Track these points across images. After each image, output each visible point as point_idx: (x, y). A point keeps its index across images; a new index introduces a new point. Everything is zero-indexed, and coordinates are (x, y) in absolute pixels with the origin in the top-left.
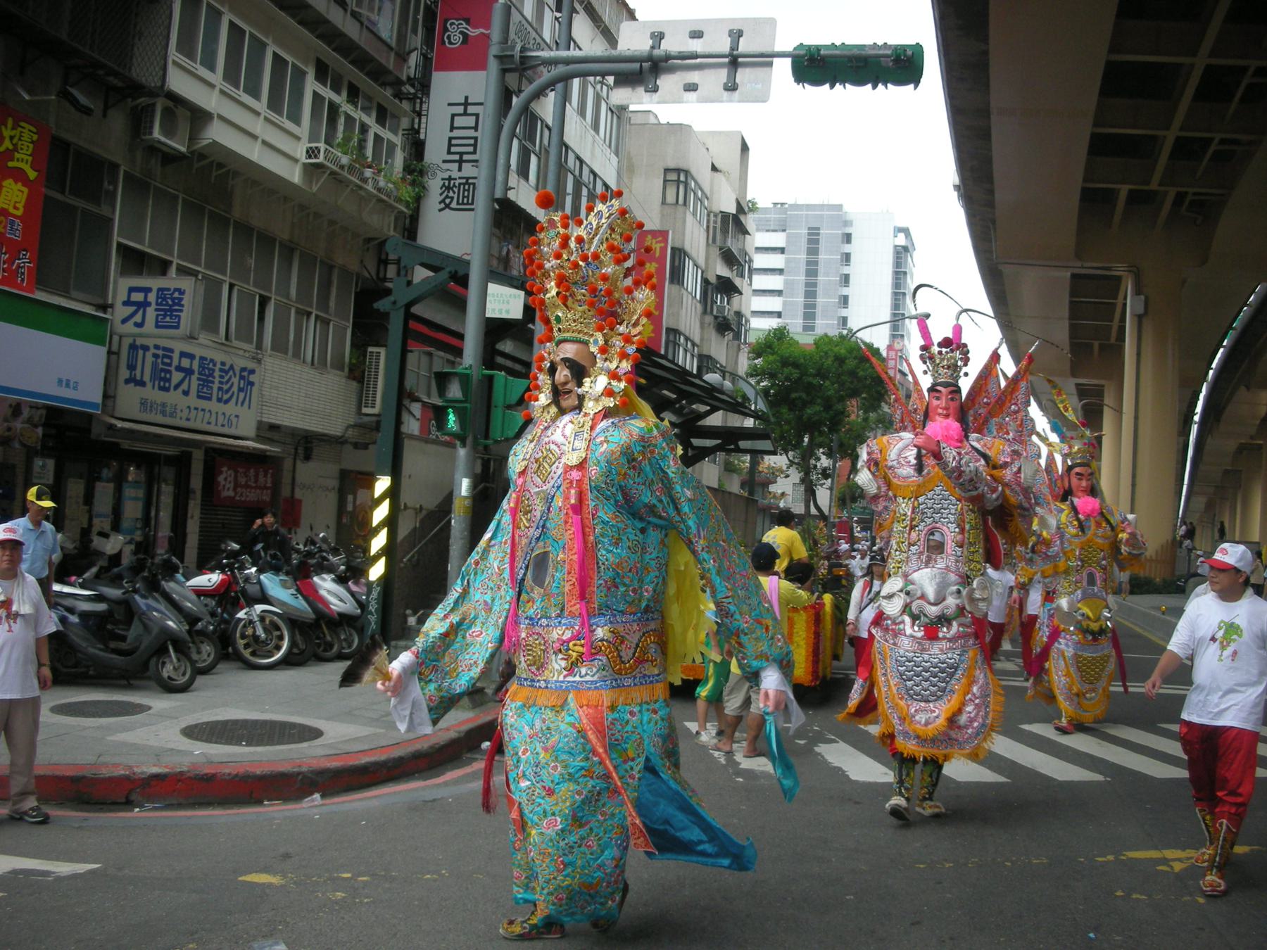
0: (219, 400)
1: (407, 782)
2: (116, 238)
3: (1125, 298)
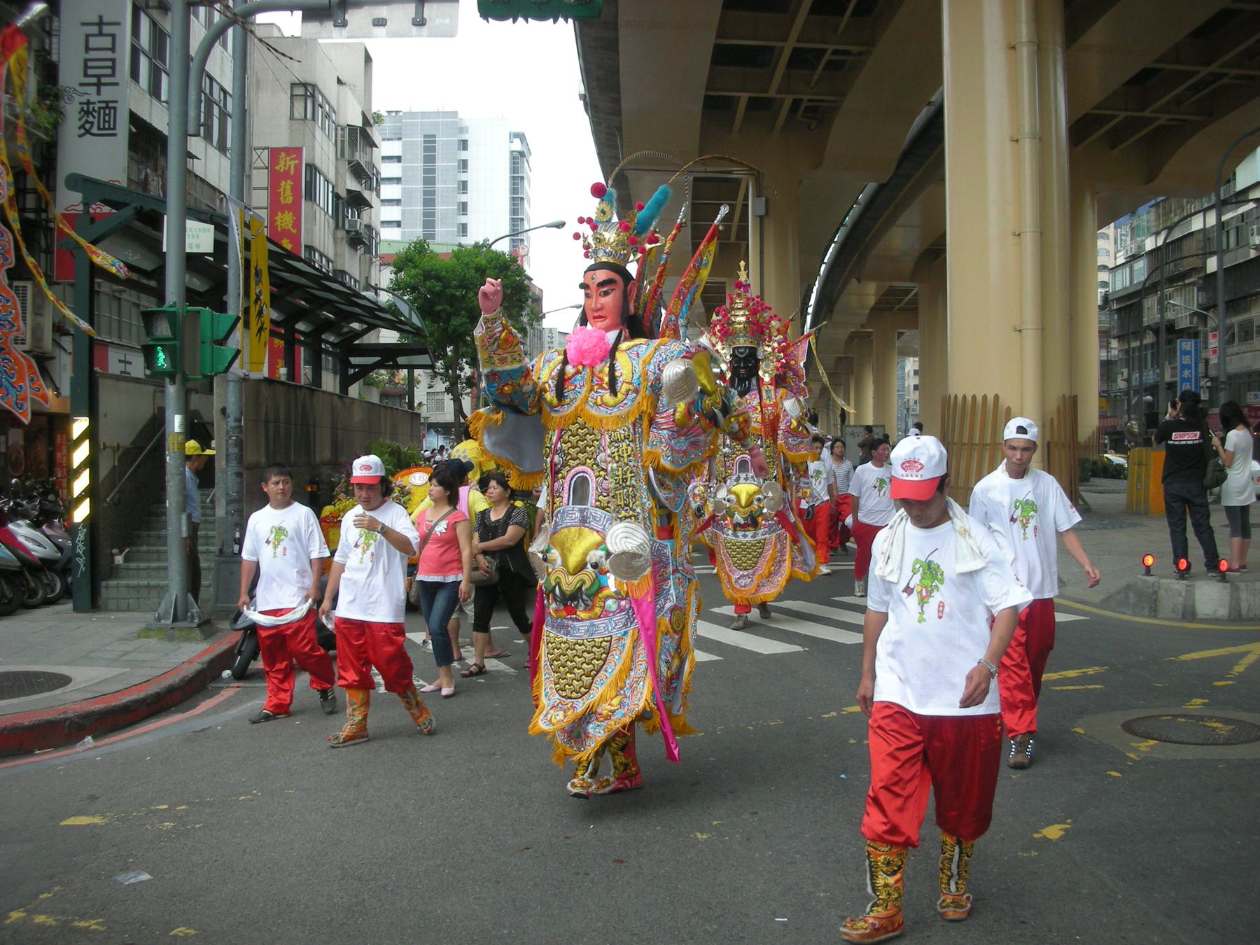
1: (167, 715)
3: (746, 198)
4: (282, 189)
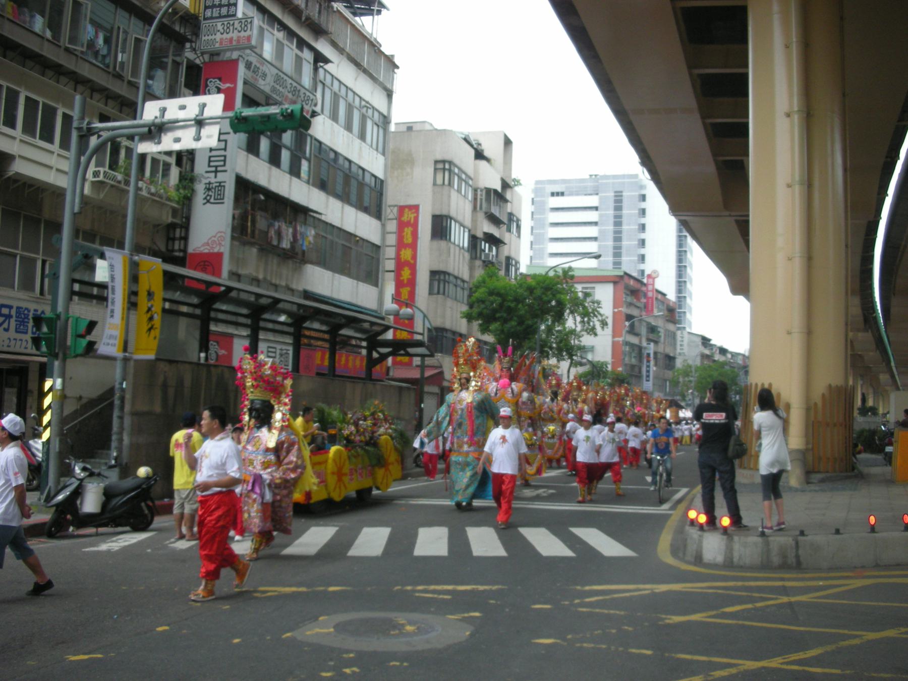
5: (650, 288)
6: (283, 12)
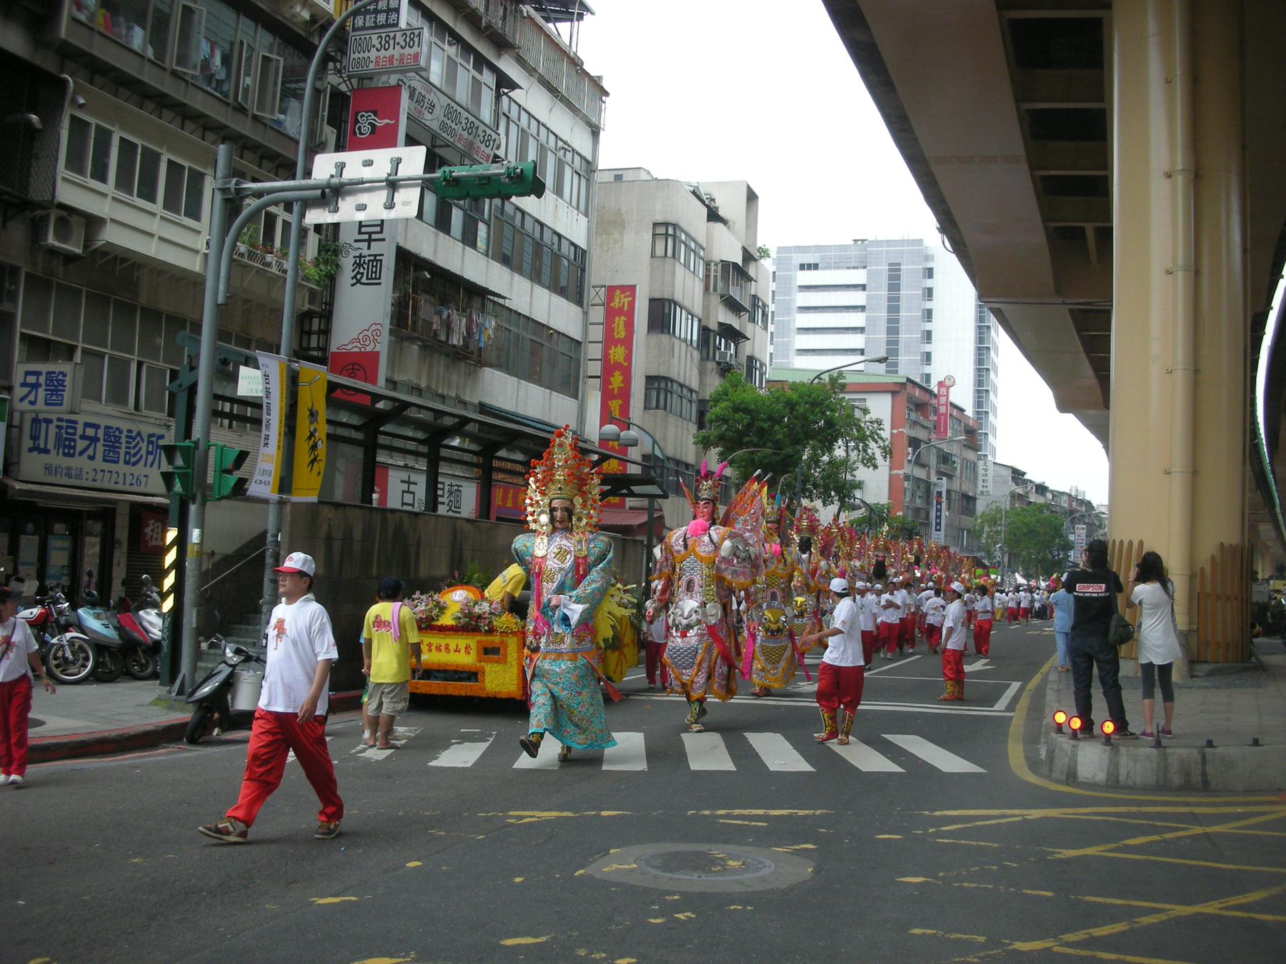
0: (127, 463)
2: (19, 329)
4: (616, 324)
5: (943, 400)
6: (456, 19)
